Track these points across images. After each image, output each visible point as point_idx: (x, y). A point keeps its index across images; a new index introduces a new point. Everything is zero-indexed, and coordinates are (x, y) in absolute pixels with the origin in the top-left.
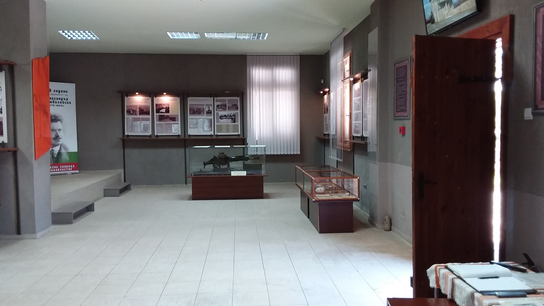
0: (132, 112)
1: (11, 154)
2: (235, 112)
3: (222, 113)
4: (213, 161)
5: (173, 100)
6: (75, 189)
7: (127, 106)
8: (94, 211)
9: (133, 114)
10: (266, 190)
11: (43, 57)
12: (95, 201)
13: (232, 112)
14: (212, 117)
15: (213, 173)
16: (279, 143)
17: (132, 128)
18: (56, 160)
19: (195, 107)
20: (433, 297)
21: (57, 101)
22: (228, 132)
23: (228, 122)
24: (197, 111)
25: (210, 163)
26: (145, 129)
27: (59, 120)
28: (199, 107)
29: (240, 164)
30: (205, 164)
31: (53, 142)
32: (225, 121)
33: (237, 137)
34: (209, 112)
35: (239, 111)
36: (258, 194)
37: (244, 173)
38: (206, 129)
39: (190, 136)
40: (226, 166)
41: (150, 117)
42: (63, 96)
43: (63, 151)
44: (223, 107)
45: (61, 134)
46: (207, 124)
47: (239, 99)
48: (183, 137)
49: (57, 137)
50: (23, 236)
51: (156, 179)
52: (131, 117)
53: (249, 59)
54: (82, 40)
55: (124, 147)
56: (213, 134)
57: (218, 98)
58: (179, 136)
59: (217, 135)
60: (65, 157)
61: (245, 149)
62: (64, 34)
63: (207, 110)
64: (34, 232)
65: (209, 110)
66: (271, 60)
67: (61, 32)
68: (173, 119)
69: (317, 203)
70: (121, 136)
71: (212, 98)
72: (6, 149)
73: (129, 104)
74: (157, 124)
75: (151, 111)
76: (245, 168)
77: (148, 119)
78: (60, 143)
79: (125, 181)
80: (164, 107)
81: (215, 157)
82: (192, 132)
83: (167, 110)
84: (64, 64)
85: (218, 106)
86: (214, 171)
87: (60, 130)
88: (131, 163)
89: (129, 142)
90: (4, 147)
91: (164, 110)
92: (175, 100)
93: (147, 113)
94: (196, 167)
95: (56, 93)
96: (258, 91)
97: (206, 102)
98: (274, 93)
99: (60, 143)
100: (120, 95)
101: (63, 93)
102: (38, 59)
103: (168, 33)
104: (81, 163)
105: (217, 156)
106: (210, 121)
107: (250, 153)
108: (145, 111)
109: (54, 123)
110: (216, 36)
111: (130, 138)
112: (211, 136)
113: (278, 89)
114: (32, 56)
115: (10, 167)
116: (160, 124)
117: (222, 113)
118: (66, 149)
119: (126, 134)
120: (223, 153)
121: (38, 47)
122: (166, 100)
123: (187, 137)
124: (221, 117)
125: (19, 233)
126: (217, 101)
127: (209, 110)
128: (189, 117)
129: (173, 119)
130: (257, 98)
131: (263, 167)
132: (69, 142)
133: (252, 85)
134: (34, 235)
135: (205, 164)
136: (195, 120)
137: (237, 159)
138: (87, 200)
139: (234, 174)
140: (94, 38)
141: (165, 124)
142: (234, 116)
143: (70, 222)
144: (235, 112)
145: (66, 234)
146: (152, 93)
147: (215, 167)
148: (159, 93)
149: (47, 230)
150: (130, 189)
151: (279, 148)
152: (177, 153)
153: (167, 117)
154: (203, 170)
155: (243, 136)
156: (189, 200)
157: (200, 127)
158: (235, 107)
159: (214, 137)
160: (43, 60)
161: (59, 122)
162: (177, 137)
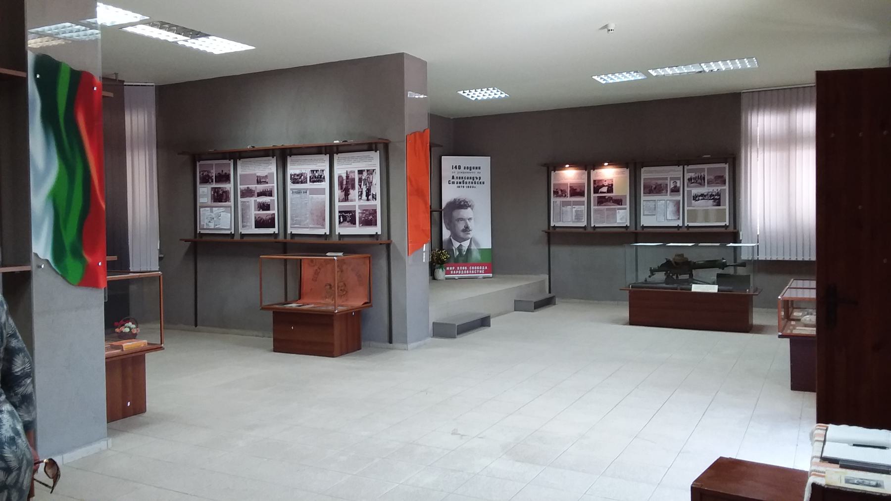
0: (560, 193)
1: (384, 247)
2: (719, 188)
3: (696, 191)
4: (668, 267)
5: (618, 173)
7: (291, 199)
8: (489, 326)
11: (422, 130)
13: (714, 189)
14: (680, 198)
15: (664, 285)
17: (560, 214)
20: (814, 485)
21: (468, 181)
23: (709, 204)
24: (656, 189)
25: (660, 269)
26: (578, 217)
28: (659, 182)
29: (713, 273)
30: (653, 272)
31: (462, 235)
32: (701, 204)
33: (723, 230)
34: (675, 190)
35: (726, 187)
36: (743, 326)
37: (714, 289)
38: (669, 217)
39: (643, 227)
40: (686, 277)
41: (585, 199)
42: (475, 174)
43: (473, 247)
44: (699, 181)
45: (471, 224)
46: (671, 208)
47: (727, 166)
48: (633, 229)
49: (467, 229)
51: (588, 292)
52: (559, 200)
53: (744, 100)
54: (488, 100)
55: (549, 243)
56: (681, 225)
57: (691, 167)
58: (626, 227)
59: (688, 227)
60: (476, 256)
61: (738, 250)
62: (465, 95)
63: (672, 186)
65: (675, 187)
66: (780, 97)
67: (461, 92)
68: (619, 202)
69: (788, 340)
70: (546, 228)
71: (681, 167)
72: (379, 241)
73: (557, 182)
75: (591, 189)
76: (721, 279)
77: (582, 203)
78: (470, 236)
79: (550, 292)
82: (646, 221)
83: (610, 189)
84: (461, 132)
85: (690, 179)
86: (666, 282)
88: (557, 266)
89: (556, 236)
91: (605, 189)
92: (622, 173)
93: (581, 194)
95: (466, 170)
96: (760, 152)
97: (670, 174)
98: (793, 153)
99: (470, 236)
100: (545, 169)
102: (415, 133)
104: (496, 263)
106: (677, 203)
107: (745, 256)
108: (578, 190)
109: (463, 210)
110: (669, 71)
111: (557, 230)
112: (678, 227)
115: (383, 262)
116: (599, 210)
117: (696, 191)
118: (477, 244)
119: (552, 224)
120: (682, 255)
121: (414, 122)
122: (608, 173)
123: (639, 229)
124: (695, 198)
125: (390, 342)
127: (675, 187)
129: (619, 202)
130: (760, 163)
131: (751, 277)
132: (480, 233)
133: (750, 141)
135: (653, 272)
138: (482, 311)
139: (696, 288)
142: (718, 194)
143: (453, 337)
144: (719, 188)
145: (445, 347)
146: (589, 164)
147: (668, 276)
148: (597, 164)
150: (555, 304)
151: (794, 250)
152: (621, 254)
153: (610, 199)
154: (649, 280)
155: (735, 227)
156: (626, 324)
157: (660, 213)
158: (720, 180)
159: (685, 230)
160: (421, 134)
161: (469, 209)
162: (623, 230)
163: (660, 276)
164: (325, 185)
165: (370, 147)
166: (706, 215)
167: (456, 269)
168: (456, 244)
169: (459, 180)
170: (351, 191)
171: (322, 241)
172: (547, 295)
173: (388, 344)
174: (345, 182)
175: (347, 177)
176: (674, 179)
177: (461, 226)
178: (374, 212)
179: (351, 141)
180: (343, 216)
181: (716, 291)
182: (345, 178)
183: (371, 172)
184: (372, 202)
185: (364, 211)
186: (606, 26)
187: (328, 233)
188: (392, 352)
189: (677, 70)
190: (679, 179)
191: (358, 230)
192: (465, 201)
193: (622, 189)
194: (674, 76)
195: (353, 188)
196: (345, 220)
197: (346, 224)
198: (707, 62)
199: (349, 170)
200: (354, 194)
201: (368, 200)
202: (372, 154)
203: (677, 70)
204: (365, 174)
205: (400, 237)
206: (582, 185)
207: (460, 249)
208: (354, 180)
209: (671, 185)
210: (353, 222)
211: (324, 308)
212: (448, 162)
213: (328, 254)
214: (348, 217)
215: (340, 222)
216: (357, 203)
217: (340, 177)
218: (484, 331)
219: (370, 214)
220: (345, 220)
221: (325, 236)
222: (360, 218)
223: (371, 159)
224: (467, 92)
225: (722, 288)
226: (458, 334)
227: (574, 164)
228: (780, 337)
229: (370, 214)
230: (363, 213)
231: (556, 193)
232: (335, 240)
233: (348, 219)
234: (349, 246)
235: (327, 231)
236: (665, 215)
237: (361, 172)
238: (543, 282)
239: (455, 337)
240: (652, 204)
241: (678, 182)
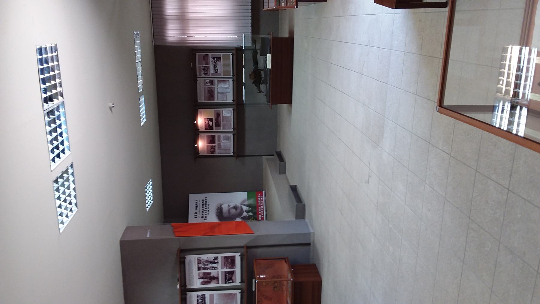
0: (213, 150)
2: (211, 58)
3: (212, 71)
5: (201, 115)
6: (277, 198)
8: (296, 186)
9: (215, 149)
10: (286, 35)
12: (288, 182)
13: (211, 61)
14: (216, 80)
15: (268, 85)
16: (240, 31)
18: (254, 214)
19: (207, 95)
21: (205, 208)
22: (230, 65)
24: (211, 93)
25: (259, 88)
26: (228, 138)
27: (221, 206)
28: (207, 91)
29: (260, 58)
30: (260, 91)
31: (239, 211)
32: (220, 68)
34: (211, 82)
35: (210, 54)
36: (290, 41)
37: (269, 57)
38: (227, 86)
40: (262, 73)
41: (216, 135)
42: (200, 203)
43: (246, 203)
45: (232, 205)
46: (222, 85)
48: (235, 107)
49: (235, 208)
50: (311, 241)
51: (273, 131)
60: (252, 201)
62: (149, 207)
64: (310, 234)
65: (209, 82)
68: (218, 115)
70: (234, 159)
71: (198, 79)
74: (223, 128)
76: (264, 54)
77: (219, 137)
78: (240, 205)
79: (273, 155)
80: (207, 122)
81: (254, 83)
82: (230, 99)
83: (210, 120)
84: (173, 209)
85: (205, 74)
86: (266, 84)
87: (229, 206)
89: (240, 151)
90: (244, 255)
91: (211, 123)
92: (201, 113)
93: (213, 137)
94: (262, 98)
95: (198, 209)
97: (202, 86)
98: (190, 18)
99: (240, 205)
101: (198, 203)
102: (174, 232)
103: (142, 124)
104: (256, 188)
105: (252, 81)
107: (250, 44)
108: (211, 139)
112: (233, 81)
113: (187, 14)
114: (172, 237)
115: (259, 250)
117: (212, 71)
118: (244, 201)
119: (232, 154)
120: (250, 75)
121: (167, 232)
122: (201, 121)
123: (235, 103)
124: (216, 71)
125: (309, 244)
126: (200, 75)
127: (209, 82)
128: (216, 101)
129: (218, 115)
131: (263, 36)
132: (239, 199)
133: (183, 41)
134: (312, 234)
135: (260, 91)
136: (219, 95)
137: (255, 61)
138: (287, 191)
139: (269, 66)
140: (151, 183)
141: (223, 121)
142: (214, 59)
143: (304, 207)
144: (211, 58)
146: (196, 133)
149: (309, 224)
150: (280, 152)
152: (249, 113)
153: (217, 120)
154: (265, 93)
155: (233, 50)
156: (291, 106)
157: (225, 91)
158: (206, 58)
159: (235, 77)
162: (235, 112)
163: (263, 87)
164: (207, 294)
165: (182, 263)
166: (227, 63)
167: (261, 214)
168: (245, 214)
169: (204, 214)
170: (212, 275)
171: (245, 295)
172: (276, 157)
173: (311, 246)
174: (206, 280)
175: (202, 278)
176: (205, 83)
177: (233, 211)
178: (226, 258)
179: (178, 276)
180: (229, 280)
181: (270, 55)
182: (202, 280)
183: (199, 261)
184: (219, 259)
185: (225, 265)
186: (110, 108)
187: (240, 291)
188: (316, 242)
189: (140, 77)
190: (205, 80)
191: (237, 269)
192: (217, 209)
193: (211, 113)
194: (144, 80)
195: (209, 273)
196: (231, 279)
197: (233, 278)
198: (135, 59)
199: (198, 277)
200: (213, 273)
201: (218, 263)
202: (187, 261)
203: (140, 77)
204: (201, 265)
205: (242, 240)
206: (208, 136)
207: (248, 212)
208: (204, 273)
209: (209, 85)
210: (232, 273)
211: (290, 290)
212: (192, 219)
213: (254, 290)
214: (229, 277)
215: (232, 282)
216: (219, 271)
217: (202, 283)
218: (300, 190)
219: (227, 261)
220: (231, 279)
221: (241, 293)
222: (230, 268)
223: (190, 261)
224: (147, 205)
225: (269, 51)
226: (301, 202)
227: (196, 142)
228: (297, 7)
229: (227, 261)
230: (227, 266)
231: (213, 152)
232: (244, 286)
233: (230, 277)
234: (248, 274)
235: (238, 292)
236: (226, 88)
237: (199, 269)
238: (267, 160)
239: (304, 205)
240: (220, 96)
241: (207, 81)
